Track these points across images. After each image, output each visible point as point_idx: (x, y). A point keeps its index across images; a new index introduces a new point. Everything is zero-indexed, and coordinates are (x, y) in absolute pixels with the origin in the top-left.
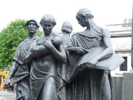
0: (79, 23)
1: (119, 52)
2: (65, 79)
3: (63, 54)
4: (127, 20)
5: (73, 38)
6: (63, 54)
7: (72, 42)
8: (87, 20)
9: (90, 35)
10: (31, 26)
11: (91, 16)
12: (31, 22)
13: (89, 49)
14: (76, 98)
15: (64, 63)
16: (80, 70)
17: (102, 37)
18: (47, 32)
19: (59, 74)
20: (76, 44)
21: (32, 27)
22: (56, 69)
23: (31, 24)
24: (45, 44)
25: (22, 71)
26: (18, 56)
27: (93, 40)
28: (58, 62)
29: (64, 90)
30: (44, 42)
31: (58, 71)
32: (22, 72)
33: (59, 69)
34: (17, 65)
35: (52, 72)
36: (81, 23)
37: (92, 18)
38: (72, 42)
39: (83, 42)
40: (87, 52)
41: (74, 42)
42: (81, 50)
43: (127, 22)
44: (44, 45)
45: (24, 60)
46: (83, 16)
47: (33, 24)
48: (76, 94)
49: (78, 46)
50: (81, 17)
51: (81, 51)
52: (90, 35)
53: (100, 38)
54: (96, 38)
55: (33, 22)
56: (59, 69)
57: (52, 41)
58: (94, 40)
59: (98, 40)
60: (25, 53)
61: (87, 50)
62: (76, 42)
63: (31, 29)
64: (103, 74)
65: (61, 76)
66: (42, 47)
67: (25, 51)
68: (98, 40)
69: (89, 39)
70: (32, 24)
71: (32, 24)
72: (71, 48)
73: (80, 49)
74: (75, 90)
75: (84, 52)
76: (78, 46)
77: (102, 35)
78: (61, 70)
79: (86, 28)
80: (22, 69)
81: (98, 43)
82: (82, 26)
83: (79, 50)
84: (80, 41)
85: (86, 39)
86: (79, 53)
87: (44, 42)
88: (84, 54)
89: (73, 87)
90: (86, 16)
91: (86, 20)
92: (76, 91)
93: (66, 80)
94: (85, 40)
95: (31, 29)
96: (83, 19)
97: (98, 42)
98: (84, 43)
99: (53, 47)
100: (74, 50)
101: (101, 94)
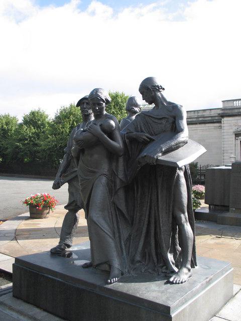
1: (156, 117)
2: (122, 179)
3: (118, 144)
6: (118, 144)
8: (153, 94)
13: (156, 135)
14: (140, 203)
15: (120, 157)
17: (175, 118)
20: (139, 128)
21: (85, 107)
23: (83, 103)
29: (121, 194)
31: (114, 167)
33: (114, 164)
35: (105, 168)
37: (161, 90)
40: (152, 140)
41: (137, 126)
42: (145, 138)
48: (139, 199)
49: (142, 131)
51: (144, 139)
53: (171, 120)
57: (101, 125)
58: (164, 121)
62: (139, 126)
69: (156, 121)
70: (85, 104)
71: (85, 104)
72: (131, 134)
73: (145, 136)
74: (137, 193)
75: (149, 140)
76: (142, 131)
78: (117, 166)
79: (153, 105)
81: (169, 126)
82: (141, 95)
89: (136, 189)
91: (152, 93)
92: (139, 194)
93: (124, 180)
96: (149, 89)
97: (173, 281)
100: (134, 137)
101: (172, 200)
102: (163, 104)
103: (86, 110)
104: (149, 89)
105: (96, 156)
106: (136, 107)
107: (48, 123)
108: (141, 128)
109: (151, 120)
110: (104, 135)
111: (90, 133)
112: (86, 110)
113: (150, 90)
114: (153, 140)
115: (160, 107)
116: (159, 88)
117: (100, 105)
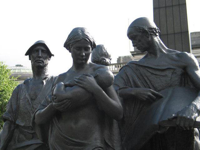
0: (135, 44)
4: (122, 59)
5: (126, 73)
7: (124, 80)
8: (150, 39)
9: (158, 66)
10: (39, 54)
11: (156, 32)
12: (38, 47)
16: (159, 132)
17: (185, 68)
18: (81, 61)
19: (107, 141)
21: (40, 55)
22: (102, 132)
23: (38, 51)
24: (84, 83)
25: (24, 138)
26: (14, 110)
27: (166, 75)
28: (105, 116)
30: (81, 80)
32: (24, 141)
33: (106, 132)
34: (12, 128)
36: (139, 43)
38: (124, 80)
39: (146, 79)
42: (150, 94)
43: (122, 62)
44: (81, 85)
45: (34, 118)
46: (144, 31)
47: (42, 51)
49: (137, 86)
50: (140, 34)
51: (149, 96)
52: (158, 66)
53: (179, 71)
54: (172, 71)
55: (43, 48)
56: (106, 132)
59: (176, 73)
60: (30, 104)
61: (160, 94)
63: (38, 59)
64: (194, 138)
65: (113, 145)
66: (77, 90)
67: (28, 100)
68: (176, 73)
69: (158, 73)
76: (137, 86)
77: (184, 64)
80: (23, 136)
81: (176, 79)
83: (144, 94)
84: (139, 78)
85: (152, 74)
86: (145, 99)
87: (81, 80)
88: (154, 100)
90: (150, 32)
94: (149, 74)
95: (38, 59)
98: (148, 81)
99: (99, 89)
102: (161, 52)
103: (41, 59)
104: (26, 55)
105: (83, 122)
106: (107, 58)
107: (133, 54)
108: (134, 81)
109: (148, 71)
110: (103, 90)
111: (81, 87)
112: (41, 59)
113: (148, 33)
114: (161, 97)
115: (158, 56)
116: (156, 31)
117: (87, 49)
